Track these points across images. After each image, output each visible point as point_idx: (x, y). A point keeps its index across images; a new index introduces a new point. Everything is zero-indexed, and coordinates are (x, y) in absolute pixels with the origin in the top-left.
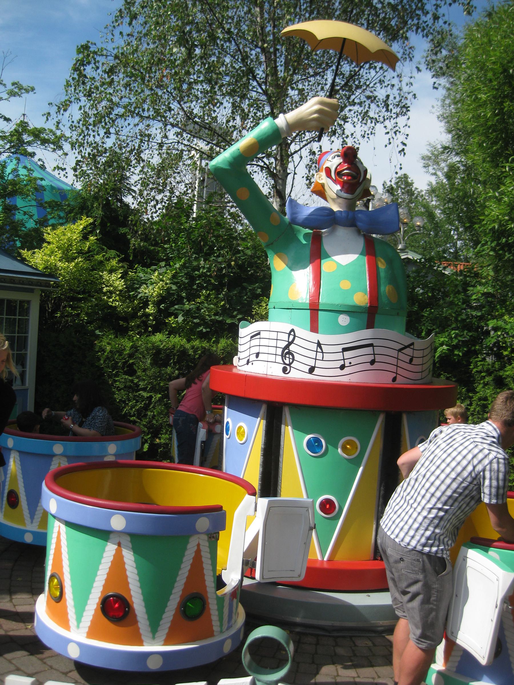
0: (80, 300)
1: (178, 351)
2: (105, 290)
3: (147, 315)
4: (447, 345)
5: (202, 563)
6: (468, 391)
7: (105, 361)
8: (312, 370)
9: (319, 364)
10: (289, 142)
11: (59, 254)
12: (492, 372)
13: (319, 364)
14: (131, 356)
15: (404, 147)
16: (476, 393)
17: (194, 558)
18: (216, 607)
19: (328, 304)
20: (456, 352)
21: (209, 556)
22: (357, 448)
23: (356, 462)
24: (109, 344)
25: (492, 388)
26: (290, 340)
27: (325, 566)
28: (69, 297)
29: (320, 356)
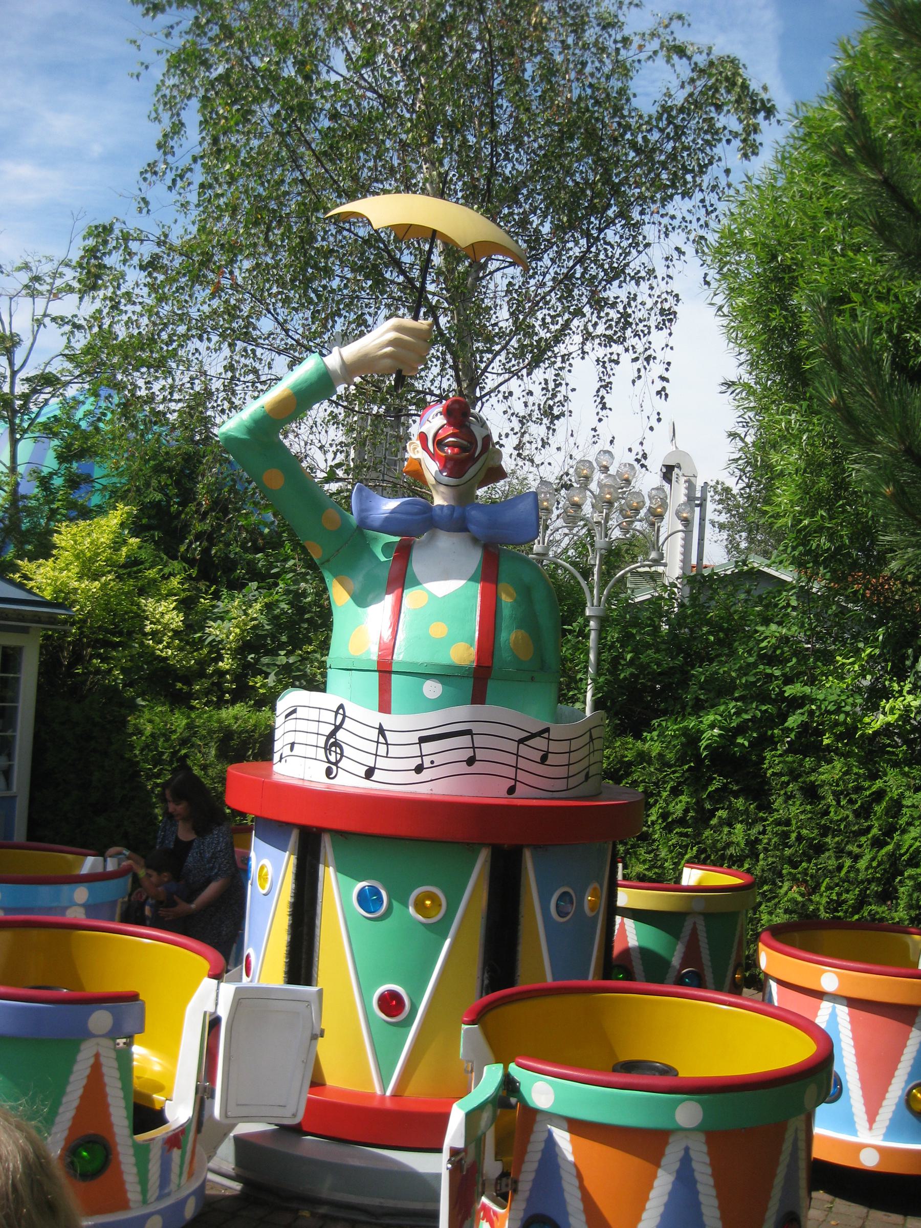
0: (115, 646)
1: (261, 735)
2: (148, 629)
3: (221, 673)
4: (720, 728)
5: (103, 1085)
6: (759, 808)
7: (142, 750)
8: (369, 773)
9: (381, 763)
10: (176, 414)
11: (75, 569)
12: (800, 776)
13: (381, 763)
14: (184, 742)
15: (665, 384)
16: (771, 811)
17: (89, 1077)
18: (133, 1160)
19: (406, 663)
20: (740, 740)
21: (117, 1074)
22: (440, 905)
23: (439, 930)
24: (150, 721)
25: (798, 803)
26: (338, 723)
27: (388, 1105)
28: (97, 641)
29: (382, 749)
